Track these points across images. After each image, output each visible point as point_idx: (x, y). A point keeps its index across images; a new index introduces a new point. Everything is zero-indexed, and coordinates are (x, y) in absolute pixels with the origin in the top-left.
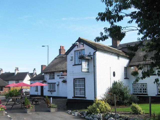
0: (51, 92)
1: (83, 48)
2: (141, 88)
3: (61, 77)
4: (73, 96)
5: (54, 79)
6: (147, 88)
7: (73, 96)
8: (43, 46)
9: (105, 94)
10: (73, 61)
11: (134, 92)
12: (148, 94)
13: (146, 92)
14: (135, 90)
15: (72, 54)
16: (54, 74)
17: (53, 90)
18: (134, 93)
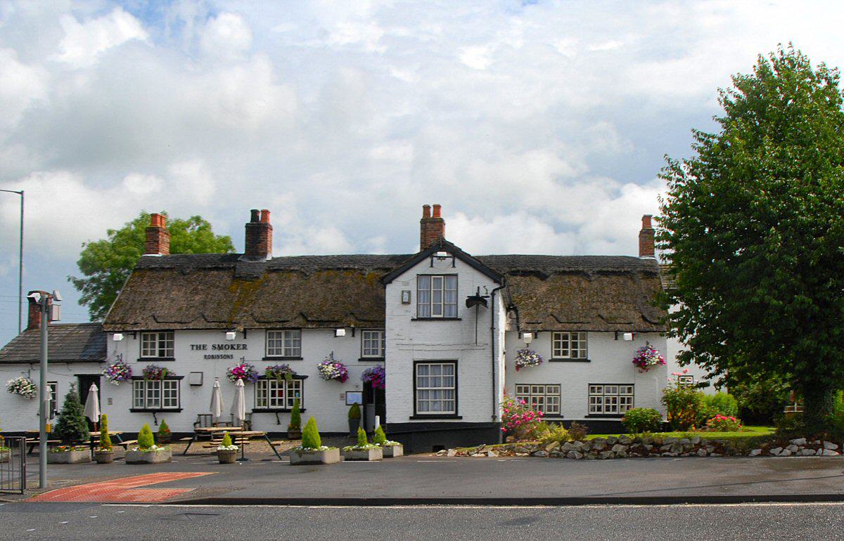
0: (157, 414)
1: (453, 271)
3: (210, 352)
10: (412, 309)
12: (562, 415)
15: (407, 284)
16: (173, 338)
17: (171, 407)
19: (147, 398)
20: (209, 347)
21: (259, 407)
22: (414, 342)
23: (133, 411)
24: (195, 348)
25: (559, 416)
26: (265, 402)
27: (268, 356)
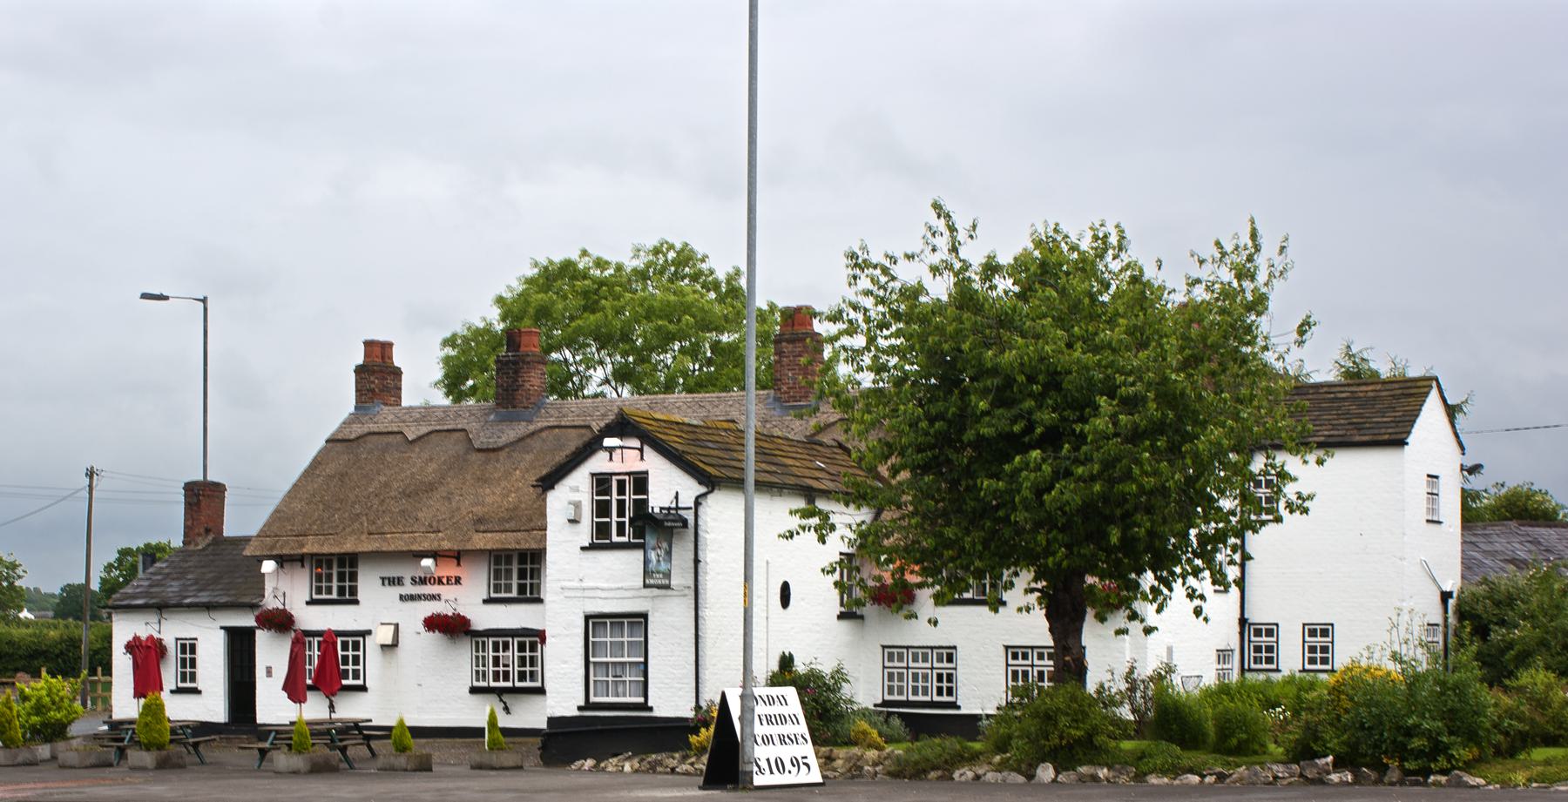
0: (506, 698)
2: (929, 671)
3: (409, 589)
4: (582, 703)
5: (356, 602)
6: (955, 669)
7: (582, 703)
8: (145, 296)
9: (1312, 458)
11: (891, 691)
13: (950, 692)
14: (896, 683)
15: (576, 490)
18: (887, 697)
19: (516, 668)
20: (407, 581)
21: (184, 685)
22: (584, 585)
23: (474, 690)
24: (386, 582)
25: (954, 705)
26: (484, 675)
27: (493, 595)
